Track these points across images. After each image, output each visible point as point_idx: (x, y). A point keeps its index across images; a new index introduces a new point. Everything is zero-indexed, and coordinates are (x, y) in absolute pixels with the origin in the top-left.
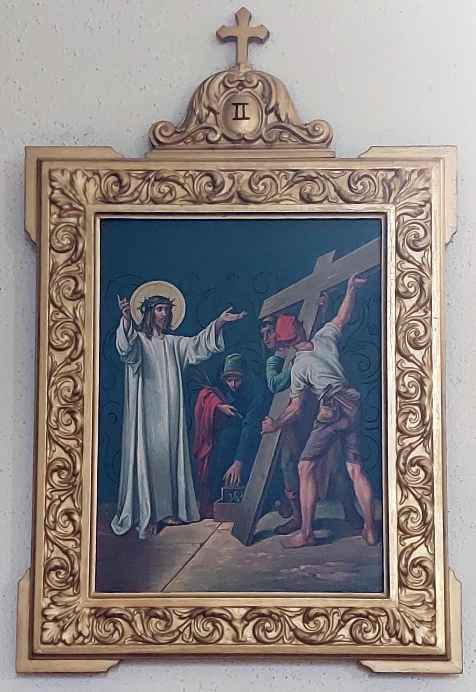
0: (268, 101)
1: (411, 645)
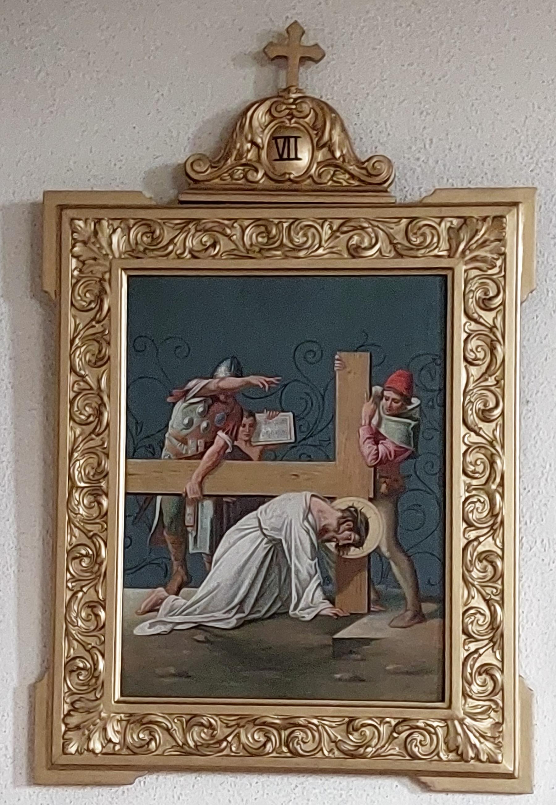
0: (320, 134)
1: (472, 762)
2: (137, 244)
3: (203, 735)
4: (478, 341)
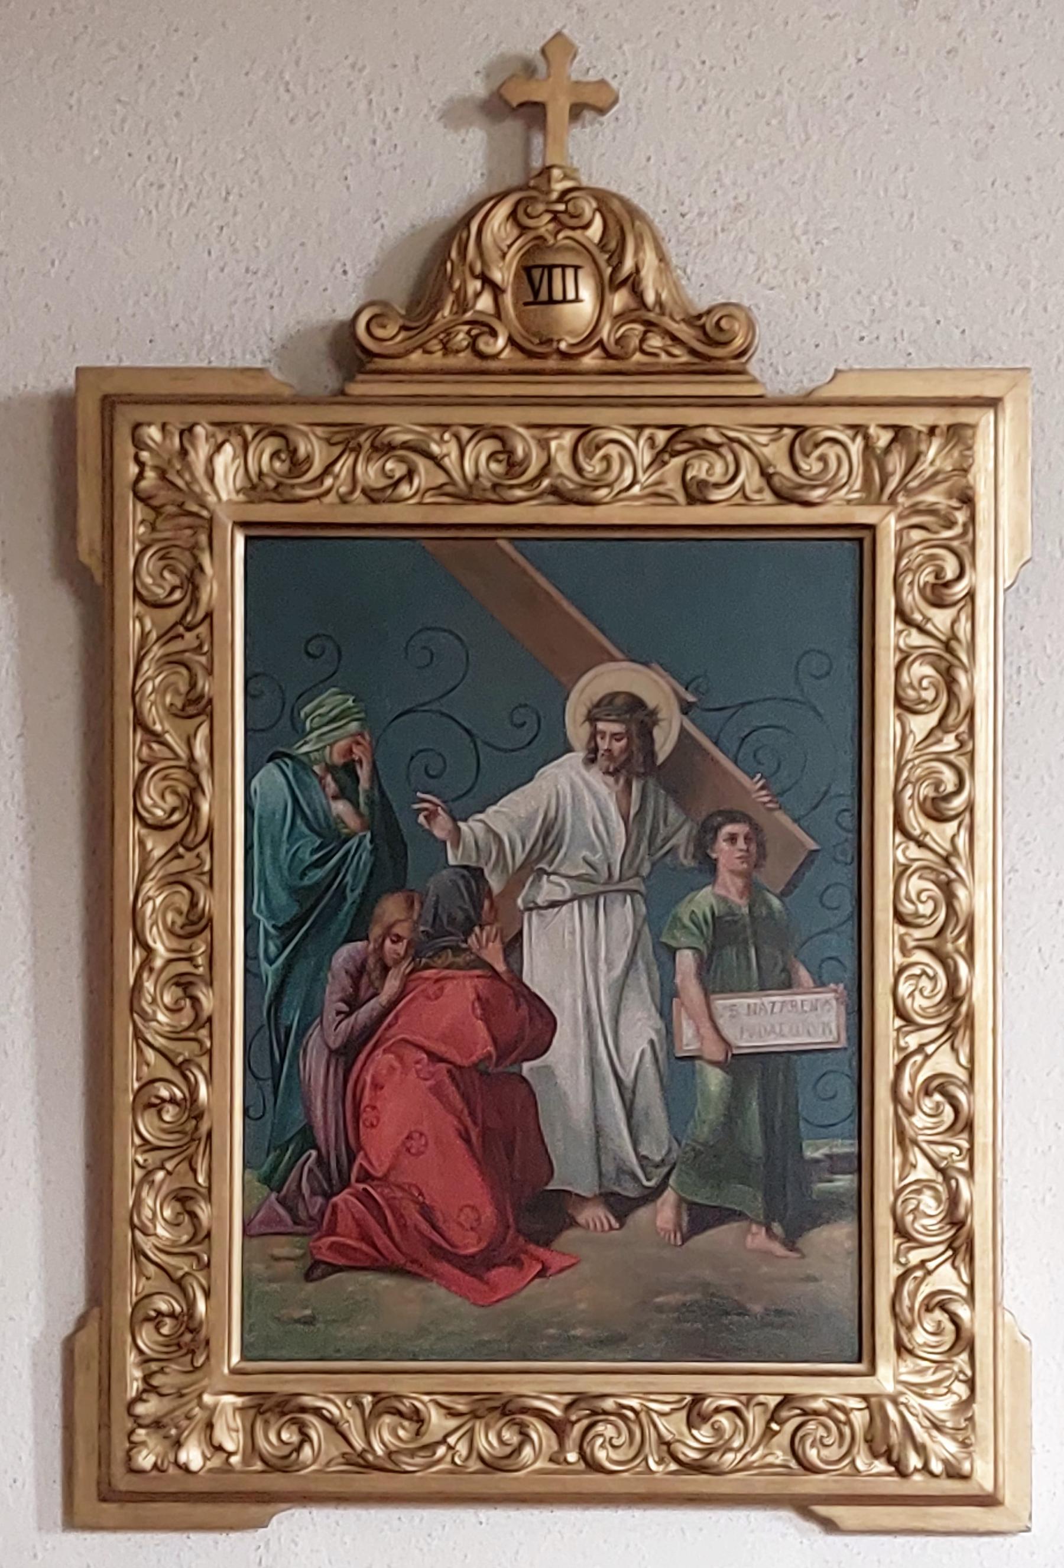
1: (917, 1477)
2: (261, 474)
3: (401, 1433)
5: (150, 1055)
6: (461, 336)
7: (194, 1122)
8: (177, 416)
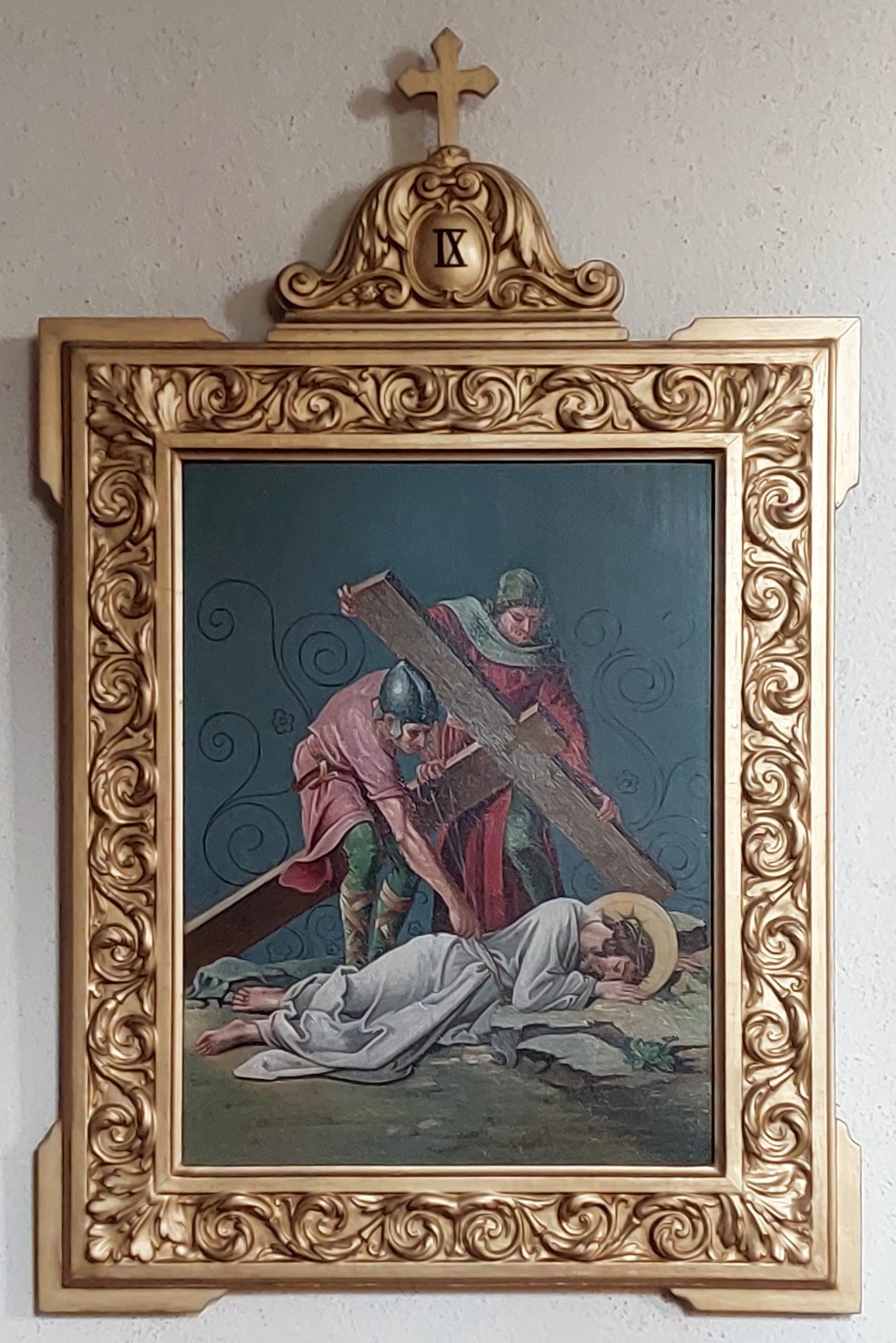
4: (768, 581)
5: (104, 904)
6: (371, 289)
7: (141, 961)
8: (123, 358)
